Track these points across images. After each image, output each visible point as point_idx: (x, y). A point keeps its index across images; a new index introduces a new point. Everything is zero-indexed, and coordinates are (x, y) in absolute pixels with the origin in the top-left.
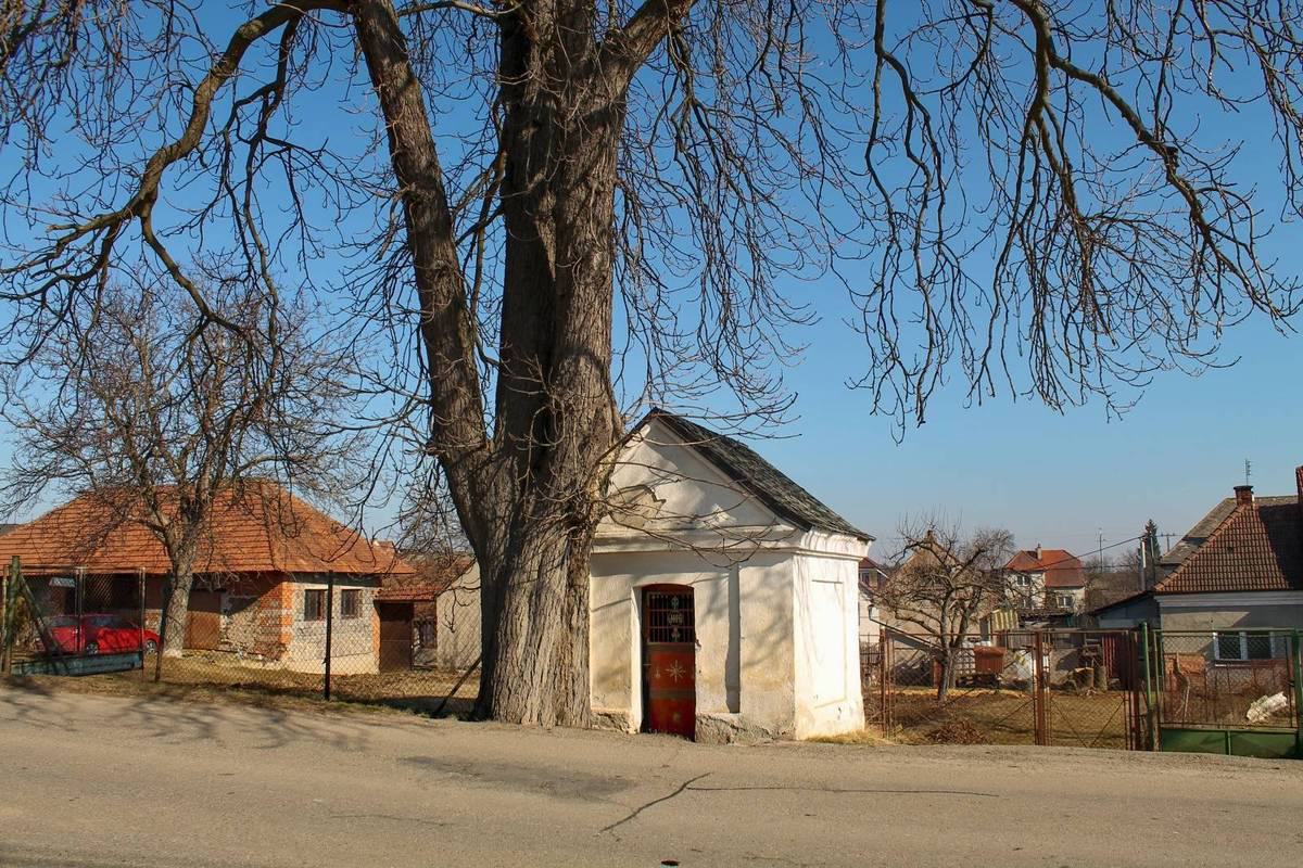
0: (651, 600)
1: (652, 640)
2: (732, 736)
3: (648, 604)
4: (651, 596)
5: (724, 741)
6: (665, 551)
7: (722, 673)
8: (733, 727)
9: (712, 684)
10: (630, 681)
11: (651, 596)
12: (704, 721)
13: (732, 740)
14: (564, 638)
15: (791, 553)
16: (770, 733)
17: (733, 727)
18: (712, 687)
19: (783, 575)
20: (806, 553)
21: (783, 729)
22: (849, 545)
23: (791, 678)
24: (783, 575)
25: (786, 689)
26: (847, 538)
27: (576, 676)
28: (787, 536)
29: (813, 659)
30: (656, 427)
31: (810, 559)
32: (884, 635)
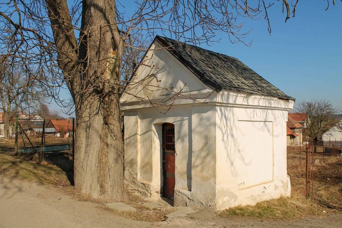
0: (167, 130)
1: (167, 150)
2: (188, 203)
3: (165, 132)
4: (166, 128)
5: (185, 205)
6: (142, 108)
7: (185, 169)
8: (188, 198)
9: (181, 175)
10: (152, 169)
11: (166, 128)
12: (177, 193)
13: (188, 205)
14: (102, 149)
15: (212, 106)
16: (204, 205)
17: (188, 198)
18: (181, 176)
19: (208, 119)
20: (234, 105)
21: (210, 204)
22: (273, 102)
23: (214, 176)
24: (208, 119)
25: (211, 181)
26: (269, 98)
27: (110, 168)
28: (209, 95)
29: (238, 162)
30: (157, 44)
31: (234, 108)
32: (308, 146)
